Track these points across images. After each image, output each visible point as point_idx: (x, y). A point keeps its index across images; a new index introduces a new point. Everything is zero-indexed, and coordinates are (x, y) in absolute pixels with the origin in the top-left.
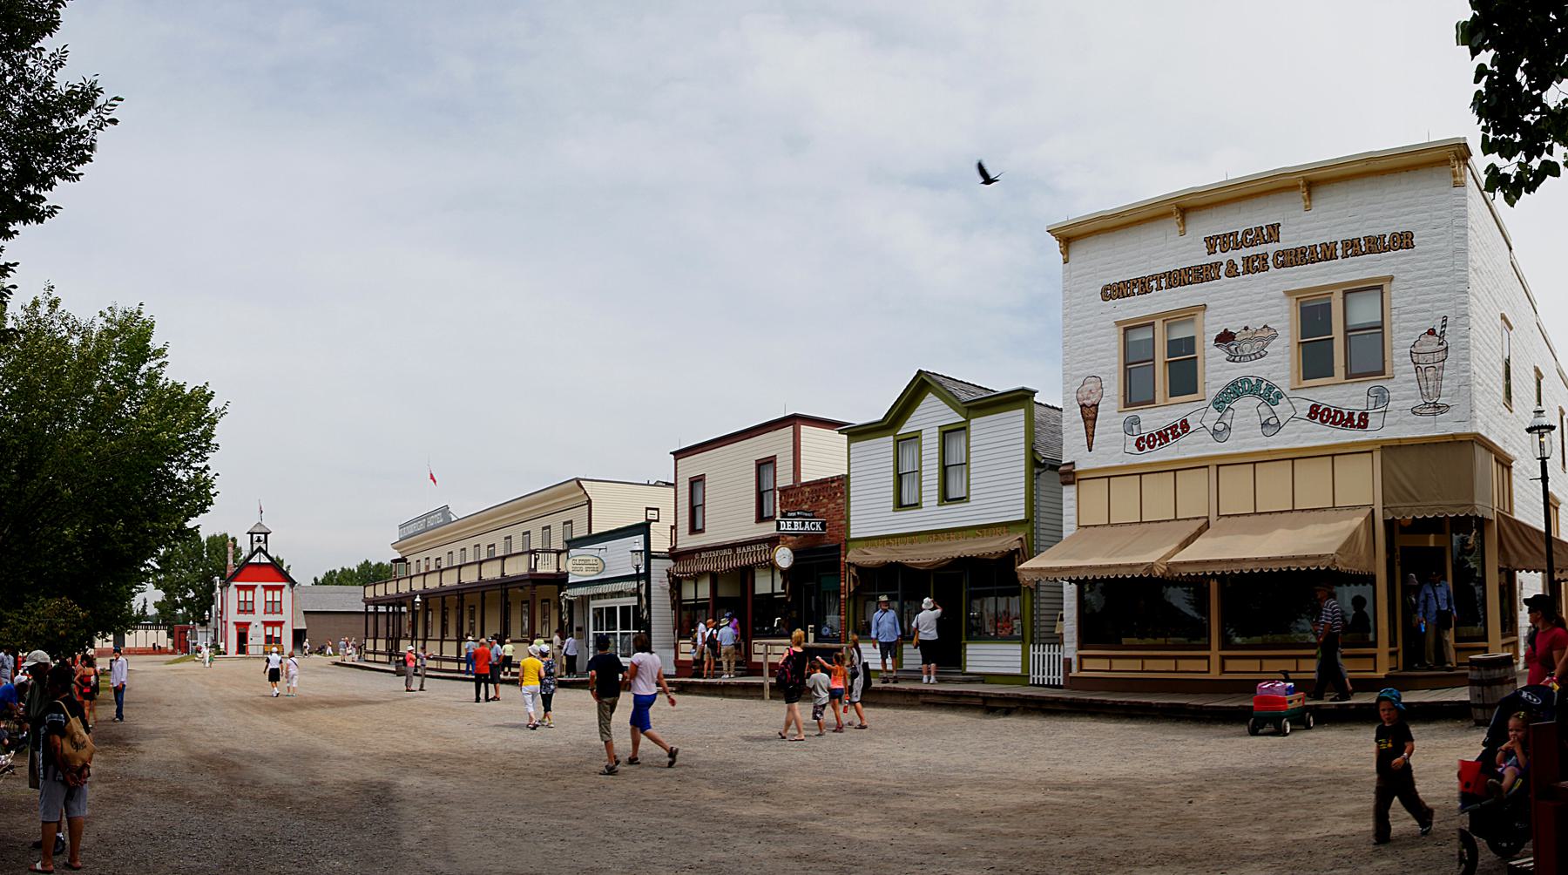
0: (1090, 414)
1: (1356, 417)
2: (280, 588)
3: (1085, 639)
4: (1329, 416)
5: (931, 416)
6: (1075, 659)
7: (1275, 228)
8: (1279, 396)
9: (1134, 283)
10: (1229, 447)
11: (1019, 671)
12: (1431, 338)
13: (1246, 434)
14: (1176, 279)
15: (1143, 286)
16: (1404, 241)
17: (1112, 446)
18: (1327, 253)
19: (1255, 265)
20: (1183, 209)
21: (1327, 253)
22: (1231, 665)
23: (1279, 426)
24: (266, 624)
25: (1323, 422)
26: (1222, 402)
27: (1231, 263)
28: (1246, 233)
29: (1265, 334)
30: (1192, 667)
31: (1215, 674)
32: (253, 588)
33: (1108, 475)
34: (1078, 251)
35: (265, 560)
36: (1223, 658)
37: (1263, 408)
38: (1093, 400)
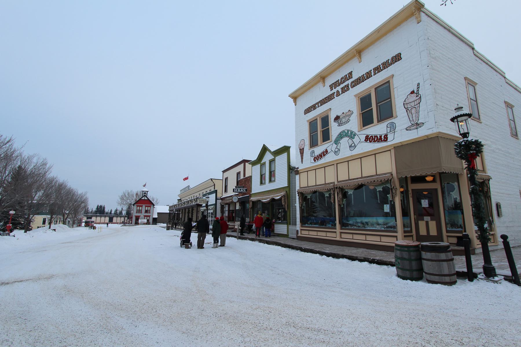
0: (302, 151)
1: (383, 137)
2: (150, 206)
3: (304, 221)
4: (372, 139)
5: (268, 156)
6: (299, 230)
7: (351, 73)
8: (355, 135)
9: (311, 107)
10: (341, 156)
11: (286, 233)
12: (412, 95)
13: (345, 152)
14: (323, 102)
15: (314, 107)
16: (397, 58)
17: (308, 162)
18: (368, 75)
19: (345, 90)
20: (322, 77)
21: (368, 75)
22: (344, 236)
23: (355, 146)
24: (145, 216)
25: (370, 142)
26: (337, 142)
27: (338, 91)
28: (342, 79)
29: (349, 113)
30: (330, 236)
31: (338, 239)
32: (142, 206)
33: (307, 171)
34: (298, 101)
35: (146, 198)
36: (341, 233)
37: (350, 141)
38: (303, 147)
